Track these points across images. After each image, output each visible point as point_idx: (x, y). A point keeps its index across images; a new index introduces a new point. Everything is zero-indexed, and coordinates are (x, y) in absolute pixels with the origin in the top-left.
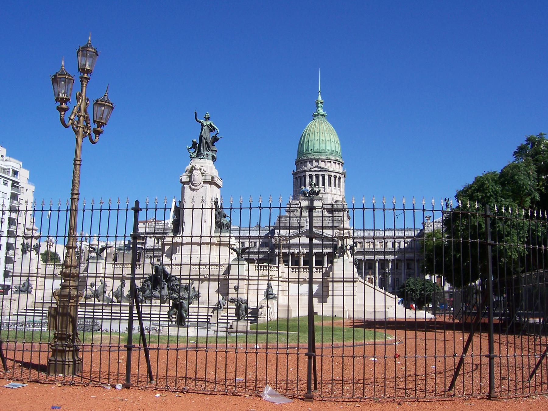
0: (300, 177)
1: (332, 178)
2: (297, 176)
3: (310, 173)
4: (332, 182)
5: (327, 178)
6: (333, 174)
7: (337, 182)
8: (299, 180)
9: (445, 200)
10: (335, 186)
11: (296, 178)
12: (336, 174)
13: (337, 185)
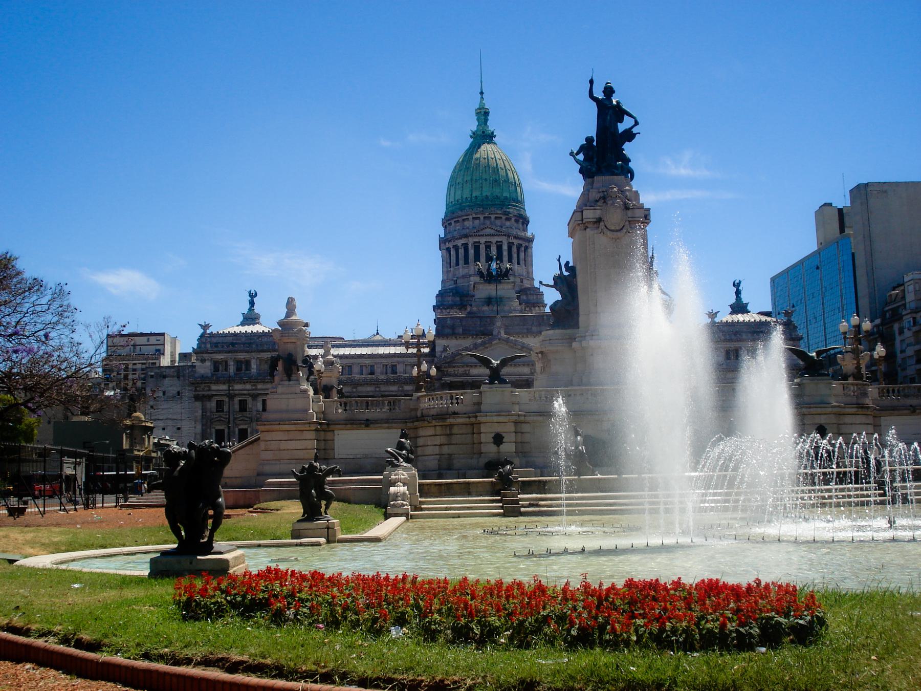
0: (456, 248)
1: (514, 249)
2: (450, 245)
3: (476, 240)
4: (515, 256)
5: (505, 247)
6: (516, 242)
7: (522, 255)
8: (453, 252)
9: (734, 285)
10: (519, 264)
11: (448, 250)
12: (520, 242)
13: (522, 262)
